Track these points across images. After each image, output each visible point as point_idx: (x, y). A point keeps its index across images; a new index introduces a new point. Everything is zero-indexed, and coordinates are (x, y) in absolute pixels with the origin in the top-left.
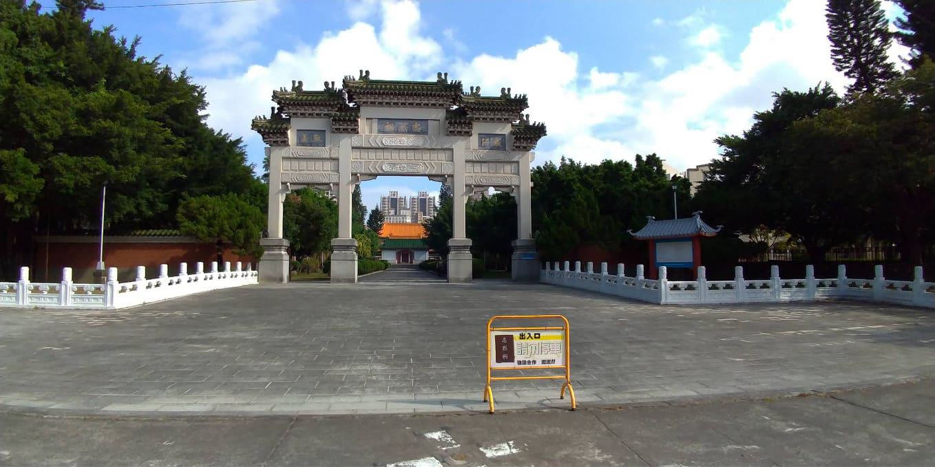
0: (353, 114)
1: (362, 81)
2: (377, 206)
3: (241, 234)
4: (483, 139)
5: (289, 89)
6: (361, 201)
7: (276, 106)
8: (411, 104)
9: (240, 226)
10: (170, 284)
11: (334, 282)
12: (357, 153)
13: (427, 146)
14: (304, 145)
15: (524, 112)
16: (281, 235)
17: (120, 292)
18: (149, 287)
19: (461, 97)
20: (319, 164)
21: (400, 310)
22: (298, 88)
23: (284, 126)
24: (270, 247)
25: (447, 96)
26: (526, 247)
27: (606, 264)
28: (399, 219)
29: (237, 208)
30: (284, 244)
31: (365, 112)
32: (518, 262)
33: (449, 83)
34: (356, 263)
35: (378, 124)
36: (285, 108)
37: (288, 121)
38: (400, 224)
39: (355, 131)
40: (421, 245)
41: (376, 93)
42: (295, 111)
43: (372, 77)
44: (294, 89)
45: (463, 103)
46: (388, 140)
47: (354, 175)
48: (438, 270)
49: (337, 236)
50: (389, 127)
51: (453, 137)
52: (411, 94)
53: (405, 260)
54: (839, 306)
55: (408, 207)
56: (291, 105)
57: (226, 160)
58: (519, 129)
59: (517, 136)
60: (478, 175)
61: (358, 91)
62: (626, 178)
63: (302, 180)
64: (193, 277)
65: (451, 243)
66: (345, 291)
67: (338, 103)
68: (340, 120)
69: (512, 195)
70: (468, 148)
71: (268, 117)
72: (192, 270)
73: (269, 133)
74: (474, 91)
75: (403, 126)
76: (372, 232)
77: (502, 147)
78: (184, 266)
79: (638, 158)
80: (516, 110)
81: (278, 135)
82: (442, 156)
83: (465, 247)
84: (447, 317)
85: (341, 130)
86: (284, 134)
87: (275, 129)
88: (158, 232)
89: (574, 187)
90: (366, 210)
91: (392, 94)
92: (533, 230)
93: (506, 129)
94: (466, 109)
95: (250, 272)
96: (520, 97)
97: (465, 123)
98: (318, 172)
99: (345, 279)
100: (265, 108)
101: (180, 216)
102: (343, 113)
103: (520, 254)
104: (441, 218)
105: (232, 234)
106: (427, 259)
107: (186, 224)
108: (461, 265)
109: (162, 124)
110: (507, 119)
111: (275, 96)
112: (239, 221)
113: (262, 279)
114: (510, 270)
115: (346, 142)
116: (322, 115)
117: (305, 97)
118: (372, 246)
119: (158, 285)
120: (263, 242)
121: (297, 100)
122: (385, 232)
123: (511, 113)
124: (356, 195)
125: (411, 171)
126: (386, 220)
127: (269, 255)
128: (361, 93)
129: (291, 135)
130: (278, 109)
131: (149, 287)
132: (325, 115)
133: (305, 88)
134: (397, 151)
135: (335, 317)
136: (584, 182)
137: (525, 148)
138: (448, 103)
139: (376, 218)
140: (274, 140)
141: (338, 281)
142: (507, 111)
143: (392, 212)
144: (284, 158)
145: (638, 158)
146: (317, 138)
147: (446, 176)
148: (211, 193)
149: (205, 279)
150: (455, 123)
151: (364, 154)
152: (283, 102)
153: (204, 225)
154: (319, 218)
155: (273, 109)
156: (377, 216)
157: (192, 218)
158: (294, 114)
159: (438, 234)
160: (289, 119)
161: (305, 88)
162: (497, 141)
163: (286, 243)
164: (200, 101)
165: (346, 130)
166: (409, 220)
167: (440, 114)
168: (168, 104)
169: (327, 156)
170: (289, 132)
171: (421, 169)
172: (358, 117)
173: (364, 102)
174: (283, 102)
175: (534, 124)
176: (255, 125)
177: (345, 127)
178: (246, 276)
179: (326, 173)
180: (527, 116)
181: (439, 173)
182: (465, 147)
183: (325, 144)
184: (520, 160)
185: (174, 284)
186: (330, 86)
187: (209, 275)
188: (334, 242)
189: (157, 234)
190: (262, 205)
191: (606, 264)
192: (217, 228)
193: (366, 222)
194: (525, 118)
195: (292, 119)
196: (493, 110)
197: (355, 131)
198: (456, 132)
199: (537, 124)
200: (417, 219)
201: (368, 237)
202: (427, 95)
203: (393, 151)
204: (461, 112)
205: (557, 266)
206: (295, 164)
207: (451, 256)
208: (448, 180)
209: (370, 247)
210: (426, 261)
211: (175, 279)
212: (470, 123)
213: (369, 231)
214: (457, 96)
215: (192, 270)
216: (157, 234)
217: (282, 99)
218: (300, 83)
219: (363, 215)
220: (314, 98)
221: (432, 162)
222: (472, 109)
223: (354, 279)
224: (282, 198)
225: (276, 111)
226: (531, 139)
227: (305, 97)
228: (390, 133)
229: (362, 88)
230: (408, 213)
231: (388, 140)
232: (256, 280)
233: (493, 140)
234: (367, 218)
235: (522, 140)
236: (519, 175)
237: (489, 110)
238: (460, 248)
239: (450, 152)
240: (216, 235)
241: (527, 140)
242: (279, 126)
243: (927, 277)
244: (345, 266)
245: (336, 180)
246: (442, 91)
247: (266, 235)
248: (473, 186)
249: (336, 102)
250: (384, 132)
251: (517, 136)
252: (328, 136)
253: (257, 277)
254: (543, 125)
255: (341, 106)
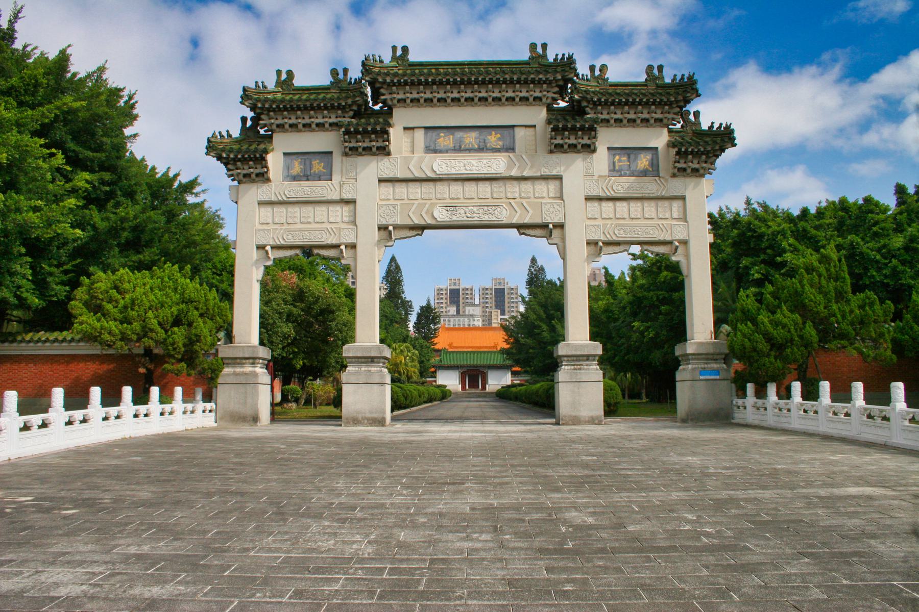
0: (381, 120)
1: (394, 64)
2: (428, 301)
3: (179, 335)
4: (617, 157)
5: (271, 85)
6: (403, 292)
7: (250, 114)
8: (483, 100)
9: (177, 322)
10: (106, 419)
11: (348, 423)
12: (388, 189)
13: (514, 173)
14: (295, 178)
15: (692, 108)
16: (255, 340)
17: (21, 430)
18: (26, 428)
19: (574, 83)
20: (321, 210)
21: (471, 499)
22: (286, 81)
23: (262, 146)
24: (236, 361)
25: (549, 83)
26: (706, 357)
27: (901, 385)
28: (464, 322)
29: (175, 290)
30: (261, 355)
31: (401, 117)
32: (690, 387)
33: (551, 58)
34: (388, 388)
35: (426, 134)
36: (263, 117)
37: (270, 138)
38: (464, 329)
39: (384, 151)
40: (498, 359)
41: (420, 83)
42: (280, 121)
43: (413, 57)
44: (279, 83)
45: (578, 92)
46: (442, 165)
47: (383, 228)
48: (543, 403)
49: (353, 339)
50: (445, 140)
51: (563, 156)
52: (484, 82)
53: (474, 384)
54: (527, 406)
55: (477, 302)
56: (274, 111)
57: (171, 216)
58: (682, 138)
59: (680, 149)
60: (609, 222)
61: (388, 80)
62: (883, 225)
63: (290, 240)
64: (113, 411)
65: (562, 349)
66: (363, 443)
67: (354, 103)
68: (357, 132)
69: (674, 258)
70: (589, 175)
71: (236, 133)
72: (111, 398)
73: (235, 160)
74: (597, 73)
75: (471, 138)
76: (421, 341)
77: (653, 171)
78: (96, 392)
79: (900, 190)
80: (677, 101)
81: (251, 163)
82: (545, 190)
83: (588, 357)
84: (590, 520)
85: (360, 150)
86: (261, 160)
87: (246, 152)
88: (53, 336)
89: (784, 244)
90: (411, 307)
91: (448, 83)
92: (718, 323)
93: (659, 139)
94: (584, 104)
95: (201, 405)
96: (682, 78)
97: (582, 129)
98: (319, 227)
99: (368, 419)
100: (231, 120)
101: (76, 306)
102: (363, 120)
103: (694, 369)
104: (532, 316)
105: (161, 334)
106: (509, 383)
107: (84, 318)
108: (582, 389)
109: (42, 141)
110: (661, 120)
111: (246, 95)
112: (176, 313)
113: (221, 419)
114: (673, 397)
115: (372, 168)
116: (327, 126)
117: (297, 97)
118: (421, 362)
119: (44, 425)
120: (225, 351)
121: (282, 101)
122: (442, 341)
123: (667, 107)
124: (393, 277)
125: (486, 218)
126: (444, 322)
127: (235, 374)
128: (394, 85)
129: (274, 161)
130: (252, 119)
131: (26, 428)
132: (331, 125)
133: (298, 82)
134: (459, 184)
135: (319, 516)
136: (803, 236)
137: (695, 171)
138: (550, 95)
139: (427, 318)
140: (245, 172)
141: (356, 421)
142: (660, 104)
143: (452, 310)
144: (261, 203)
145: (900, 190)
146: (318, 166)
147: (551, 226)
148: (139, 267)
149: (136, 416)
150: (565, 129)
151: (401, 189)
152: (259, 105)
153: (115, 320)
154: (327, 312)
155: (244, 120)
156: (428, 315)
157: (95, 308)
158: (278, 126)
159: (529, 341)
160: (271, 137)
161: (298, 82)
162: (643, 161)
163: (265, 353)
164: (128, 115)
165: (368, 150)
166: (478, 323)
167: (539, 115)
168: (58, 108)
169: (335, 196)
170: (270, 158)
171: (504, 215)
172: (390, 125)
173: (399, 101)
174: (259, 105)
175: (712, 126)
176: (214, 147)
177: (365, 145)
178: (192, 412)
179: (333, 226)
180: (697, 114)
181: (538, 220)
182: (585, 173)
183: (331, 175)
184: (689, 195)
185: (77, 424)
186: (341, 76)
187: (142, 409)
188: (348, 351)
189: (51, 338)
190: (224, 286)
191: (901, 385)
192: (136, 326)
193: (411, 326)
194: (692, 117)
195: (274, 135)
196: (633, 104)
197: (384, 151)
198: (566, 147)
199: (716, 126)
200: (490, 319)
201: (414, 347)
202: (512, 82)
203: (453, 184)
204: (576, 110)
205: (772, 389)
206: (281, 211)
207: (563, 374)
208: (554, 232)
209: (416, 363)
210: (509, 386)
211: (78, 414)
212: (592, 129)
213: (416, 339)
214: (567, 81)
215: (111, 398)
216: (51, 338)
217: (258, 100)
218: (290, 74)
219: (407, 314)
220: (312, 97)
221: (524, 202)
222: (595, 104)
223: (384, 419)
224: (258, 274)
225: (249, 123)
226: (707, 153)
227: (297, 97)
228: (447, 151)
229: (396, 75)
230: (478, 311)
231: (442, 165)
232: (213, 419)
233: (636, 159)
234: (413, 319)
235: (690, 157)
236: (686, 221)
237: (626, 103)
238: (579, 359)
239: (557, 183)
240: (135, 337)
241: (700, 157)
242: (253, 147)
243: (911, 401)
244: (366, 392)
245: (350, 240)
246: (539, 73)
247: (230, 338)
248: (601, 244)
249: (350, 101)
250: (435, 151)
251: (680, 149)
252: (337, 159)
253: (213, 414)
254: (728, 127)
255: (359, 110)
